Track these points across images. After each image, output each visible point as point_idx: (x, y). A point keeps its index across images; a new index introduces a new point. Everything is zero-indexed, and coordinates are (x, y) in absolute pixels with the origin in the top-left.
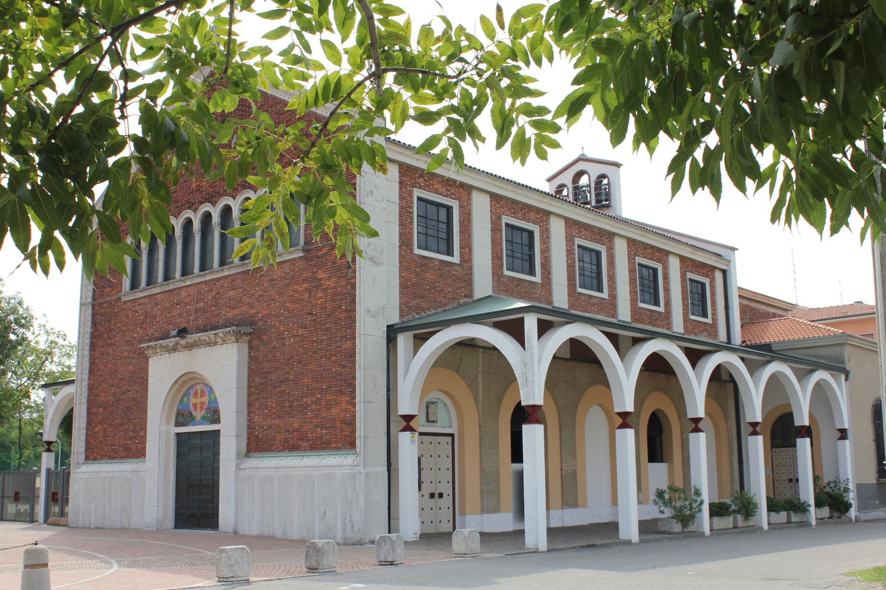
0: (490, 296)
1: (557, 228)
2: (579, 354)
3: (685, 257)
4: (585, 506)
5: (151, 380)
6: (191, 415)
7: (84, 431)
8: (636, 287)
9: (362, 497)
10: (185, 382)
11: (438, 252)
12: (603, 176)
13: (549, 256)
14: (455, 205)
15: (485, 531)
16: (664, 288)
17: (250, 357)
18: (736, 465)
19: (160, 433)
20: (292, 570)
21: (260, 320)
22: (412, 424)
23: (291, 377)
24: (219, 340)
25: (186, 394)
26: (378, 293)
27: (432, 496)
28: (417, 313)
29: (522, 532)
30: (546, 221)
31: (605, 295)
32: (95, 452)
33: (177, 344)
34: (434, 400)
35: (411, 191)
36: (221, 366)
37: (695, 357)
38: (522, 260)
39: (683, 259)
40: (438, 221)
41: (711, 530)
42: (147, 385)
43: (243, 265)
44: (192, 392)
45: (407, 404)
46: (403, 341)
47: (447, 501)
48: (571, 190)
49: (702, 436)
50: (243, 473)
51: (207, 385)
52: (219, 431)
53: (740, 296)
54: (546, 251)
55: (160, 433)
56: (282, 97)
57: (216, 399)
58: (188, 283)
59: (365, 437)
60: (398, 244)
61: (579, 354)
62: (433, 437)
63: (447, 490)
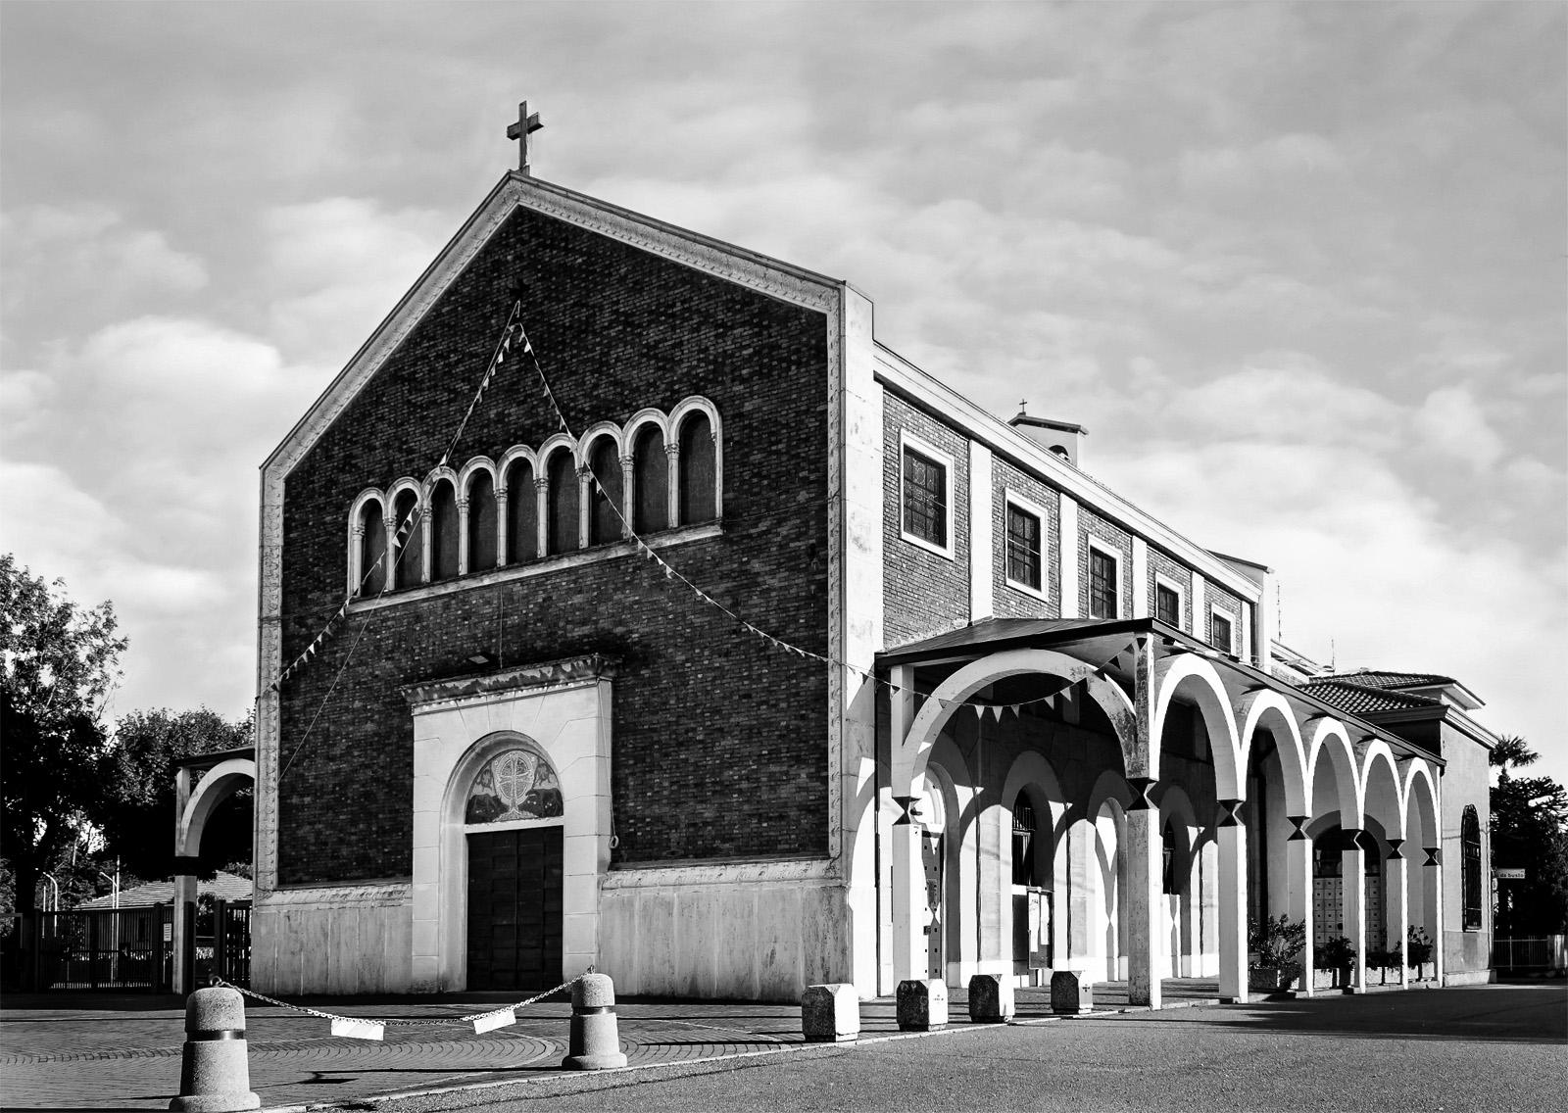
7: (275, 836)
24: (562, 677)
36: (566, 727)
50: (608, 895)
52: (561, 828)
55: (439, 834)
58: (487, 582)
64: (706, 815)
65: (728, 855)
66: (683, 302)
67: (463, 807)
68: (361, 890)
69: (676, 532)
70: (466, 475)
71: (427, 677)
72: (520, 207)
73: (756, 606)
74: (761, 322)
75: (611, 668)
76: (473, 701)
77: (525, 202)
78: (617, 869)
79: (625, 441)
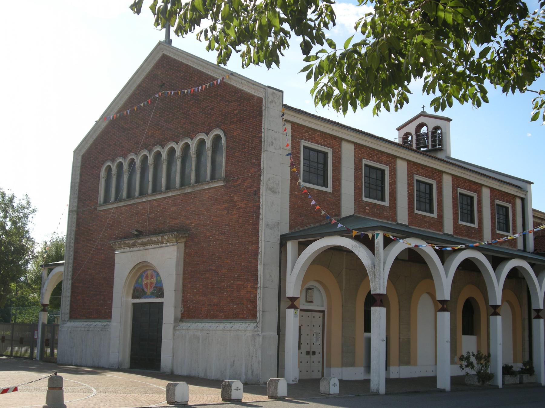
0: (353, 216)
1: (402, 168)
2: (412, 257)
3: (494, 189)
4: (415, 364)
5: (117, 266)
6: (143, 290)
7: (69, 299)
8: (458, 210)
9: (260, 352)
10: (140, 268)
11: (317, 184)
12: (438, 128)
13: (395, 188)
14: (330, 152)
15: (344, 379)
16: (478, 210)
17: (185, 253)
18: (527, 338)
19: (122, 302)
20: (197, 400)
21: (193, 228)
22: (296, 303)
23: (213, 268)
24: (164, 241)
25: (141, 276)
26: (274, 210)
27: (308, 353)
28: (301, 227)
29: (368, 381)
30: (393, 163)
31: (435, 215)
32: (76, 314)
33: (135, 242)
34: (311, 287)
35: (299, 143)
36: (166, 259)
37: (497, 262)
38: (376, 190)
39: (492, 190)
40: (318, 163)
41: (503, 384)
42: (114, 269)
43: (182, 189)
44: (145, 275)
45: (292, 290)
46: (291, 246)
47: (317, 358)
48: (414, 137)
49: (499, 318)
50: (178, 332)
51: (156, 271)
53: (534, 216)
54: (393, 184)
55: (122, 302)
56: (212, 75)
57: (161, 281)
58: (144, 200)
59: (263, 311)
60: (289, 179)
61: (412, 257)
62: (310, 313)
63: (318, 349)
64: (214, 301)
65: (222, 318)
66: (215, 92)
67: (131, 292)
68: (96, 323)
69: (208, 183)
70: (140, 157)
71: (121, 238)
72: (164, 54)
73: (235, 214)
74: (241, 100)
75: (184, 238)
76: (135, 249)
77: (165, 53)
78: (182, 322)
79: (193, 145)
